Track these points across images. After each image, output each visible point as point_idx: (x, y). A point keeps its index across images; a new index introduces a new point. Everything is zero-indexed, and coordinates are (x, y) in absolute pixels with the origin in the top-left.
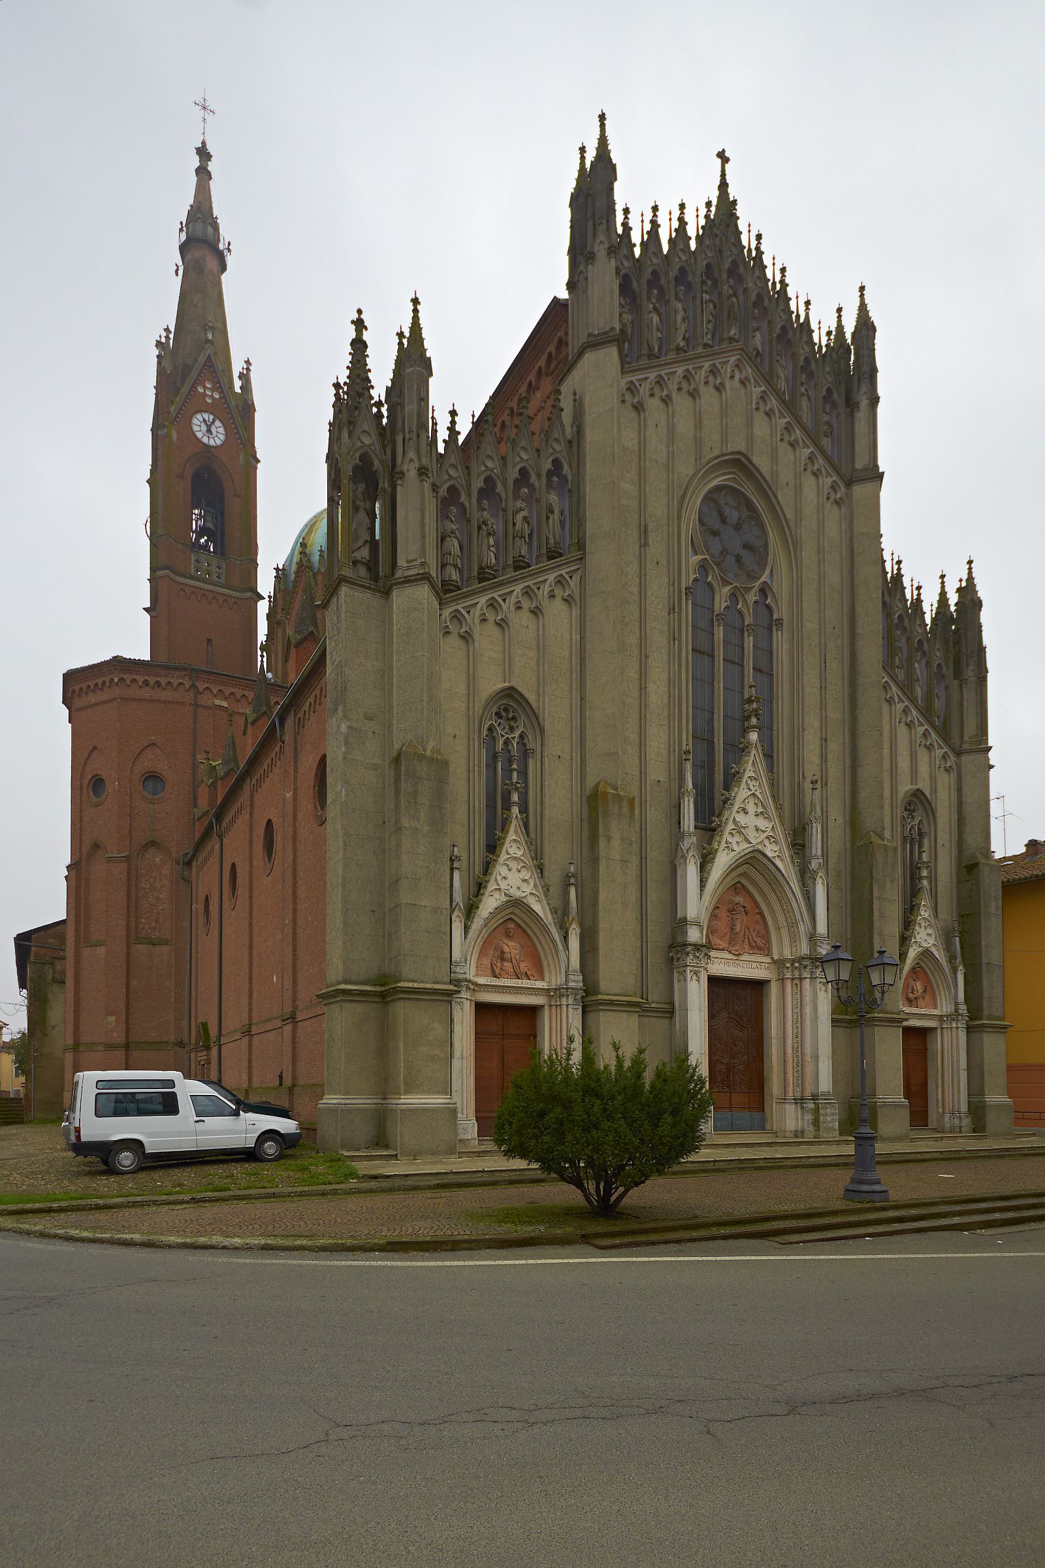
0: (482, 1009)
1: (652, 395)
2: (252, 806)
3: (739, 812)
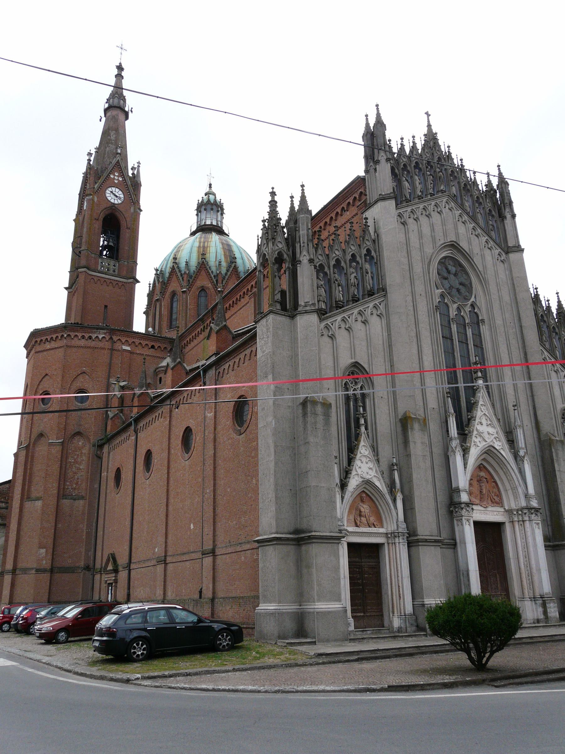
0: (351, 546)
1: (409, 217)
2: (170, 416)
3: (478, 424)
